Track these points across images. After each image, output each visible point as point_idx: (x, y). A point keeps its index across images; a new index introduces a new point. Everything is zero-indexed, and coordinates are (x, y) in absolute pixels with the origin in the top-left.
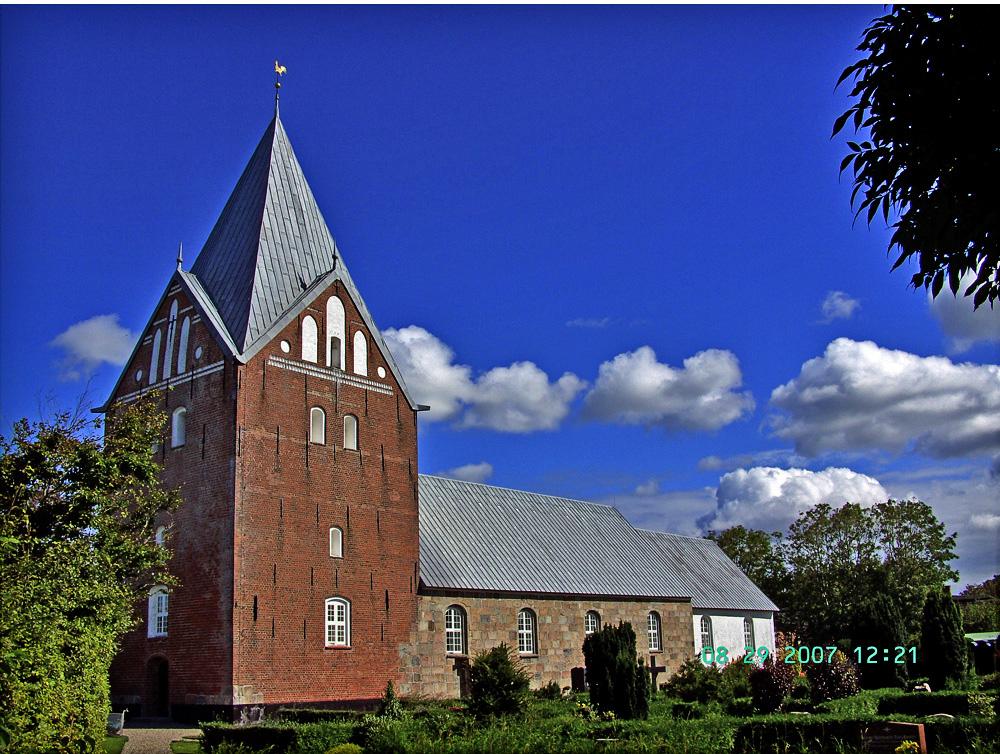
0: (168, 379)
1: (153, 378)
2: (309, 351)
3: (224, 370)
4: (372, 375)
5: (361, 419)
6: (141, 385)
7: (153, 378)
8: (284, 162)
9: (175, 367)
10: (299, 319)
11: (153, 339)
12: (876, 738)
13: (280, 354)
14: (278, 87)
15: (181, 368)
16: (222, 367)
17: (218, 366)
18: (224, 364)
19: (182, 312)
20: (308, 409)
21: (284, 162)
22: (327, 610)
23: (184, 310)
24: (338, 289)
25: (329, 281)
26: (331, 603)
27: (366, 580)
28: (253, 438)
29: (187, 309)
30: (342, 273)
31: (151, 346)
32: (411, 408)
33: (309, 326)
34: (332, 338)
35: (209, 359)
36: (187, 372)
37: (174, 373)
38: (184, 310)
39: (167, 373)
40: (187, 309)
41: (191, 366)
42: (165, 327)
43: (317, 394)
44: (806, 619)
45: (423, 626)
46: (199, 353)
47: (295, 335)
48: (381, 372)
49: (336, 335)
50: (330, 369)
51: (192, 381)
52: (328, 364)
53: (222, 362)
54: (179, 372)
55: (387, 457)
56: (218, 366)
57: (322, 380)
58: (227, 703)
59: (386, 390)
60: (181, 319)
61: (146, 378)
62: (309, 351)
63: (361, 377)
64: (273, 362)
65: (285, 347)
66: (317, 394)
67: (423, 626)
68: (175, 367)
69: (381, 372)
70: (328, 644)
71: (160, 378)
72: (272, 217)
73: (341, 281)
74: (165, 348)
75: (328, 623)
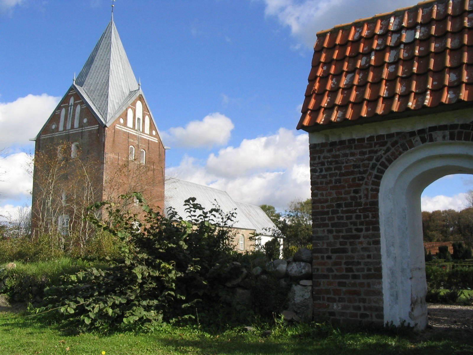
0: (69, 130)
1: (61, 128)
2: (130, 124)
3: (98, 129)
4: (151, 134)
5: (147, 151)
6: (53, 131)
7: (61, 128)
8: (114, 27)
10: (127, 110)
11: (60, 112)
13: (120, 124)
14: (112, 7)
16: (97, 128)
17: (95, 127)
18: (99, 127)
20: (129, 146)
21: (114, 27)
23: (77, 102)
24: (140, 98)
25: (138, 95)
29: (79, 101)
30: (141, 92)
32: (164, 148)
33: (130, 113)
34: (346, 272)
35: (90, 123)
36: (79, 128)
37: (72, 127)
38: (77, 102)
40: (79, 101)
41: (81, 125)
42: (67, 108)
43: (132, 141)
46: (85, 121)
48: (154, 133)
49: (139, 117)
50: (136, 131)
51: (82, 132)
52: (136, 129)
53: (97, 126)
54: (67, 128)
56: (95, 127)
57: (134, 135)
59: (155, 140)
60: (75, 105)
61: (57, 128)
62: (130, 124)
63: (146, 134)
64: (118, 127)
65: (122, 121)
66: (132, 141)
69: (154, 133)
72: (113, 65)
73: (142, 95)
74: (74, 118)
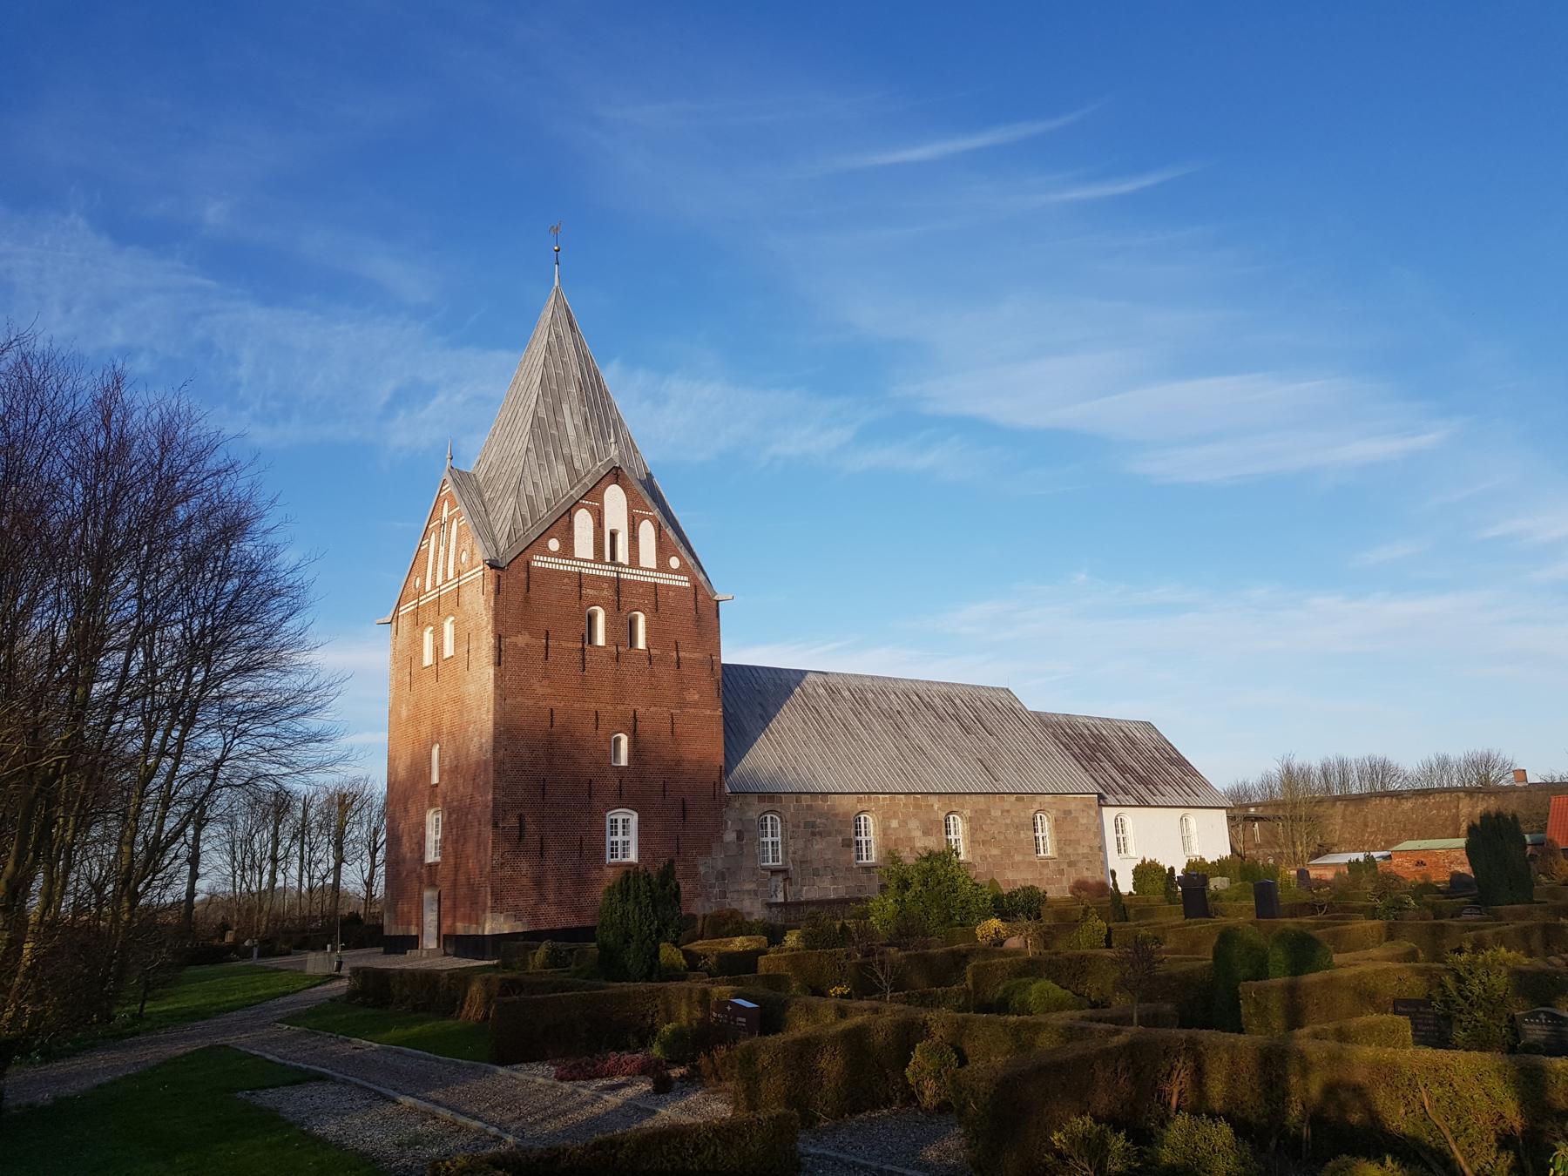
4: (663, 566)
9: (445, 574)
11: (429, 543)
12: (183, 905)
15: (451, 575)
19: (451, 513)
22: (608, 824)
23: (453, 511)
26: (613, 817)
27: (656, 789)
28: (516, 645)
31: (427, 550)
33: (583, 522)
38: (453, 511)
39: (439, 581)
44: (1438, 809)
45: (730, 836)
47: (563, 526)
55: (682, 654)
57: (599, 577)
58: (480, 933)
59: (683, 582)
64: (539, 562)
67: (730, 836)
68: (445, 574)
70: (609, 860)
71: (434, 586)
75: (610, 839)
